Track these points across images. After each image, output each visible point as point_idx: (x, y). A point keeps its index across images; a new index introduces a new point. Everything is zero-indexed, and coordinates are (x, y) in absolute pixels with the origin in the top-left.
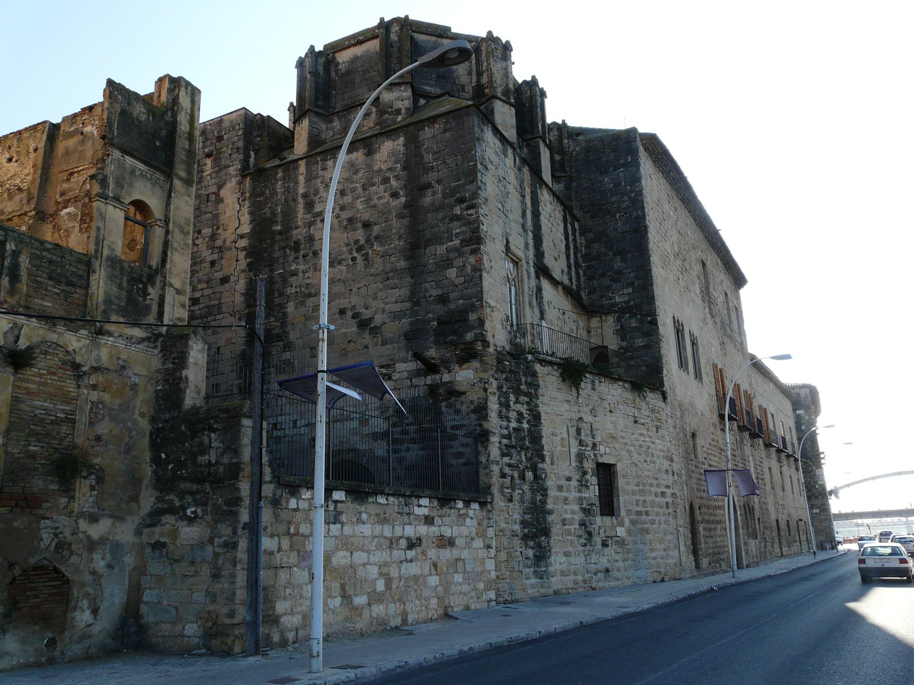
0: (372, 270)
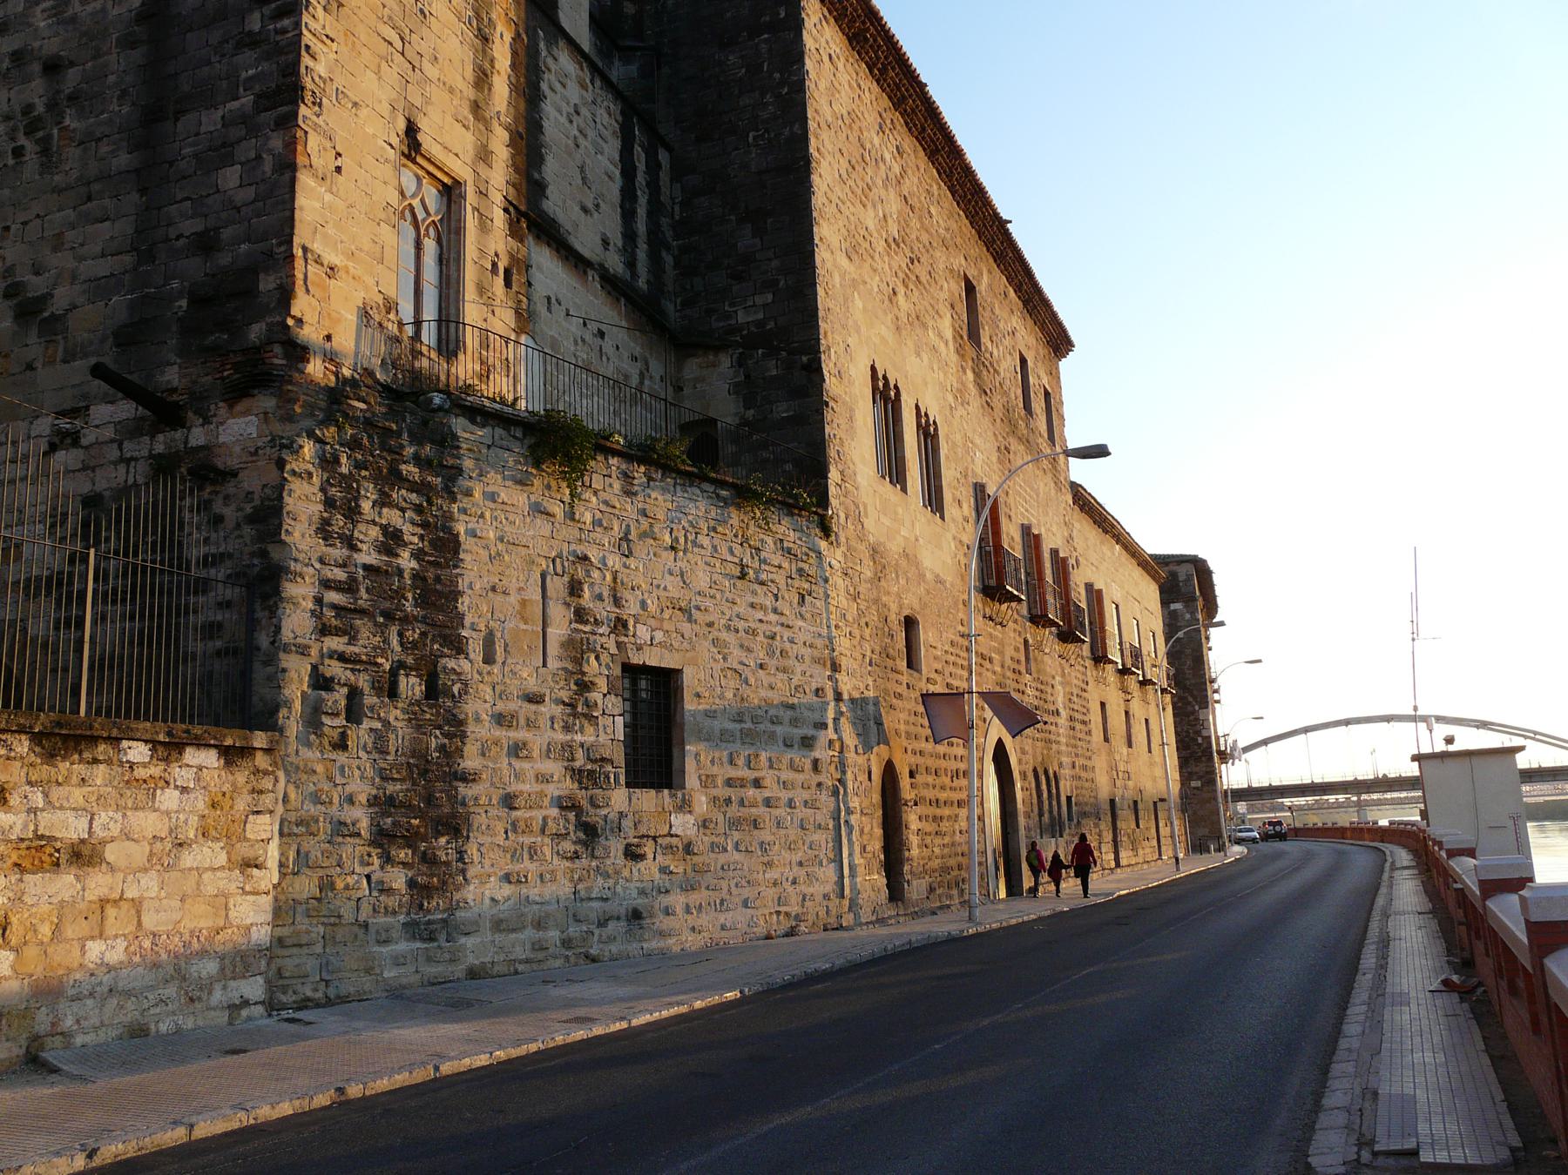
0: (56, 178)
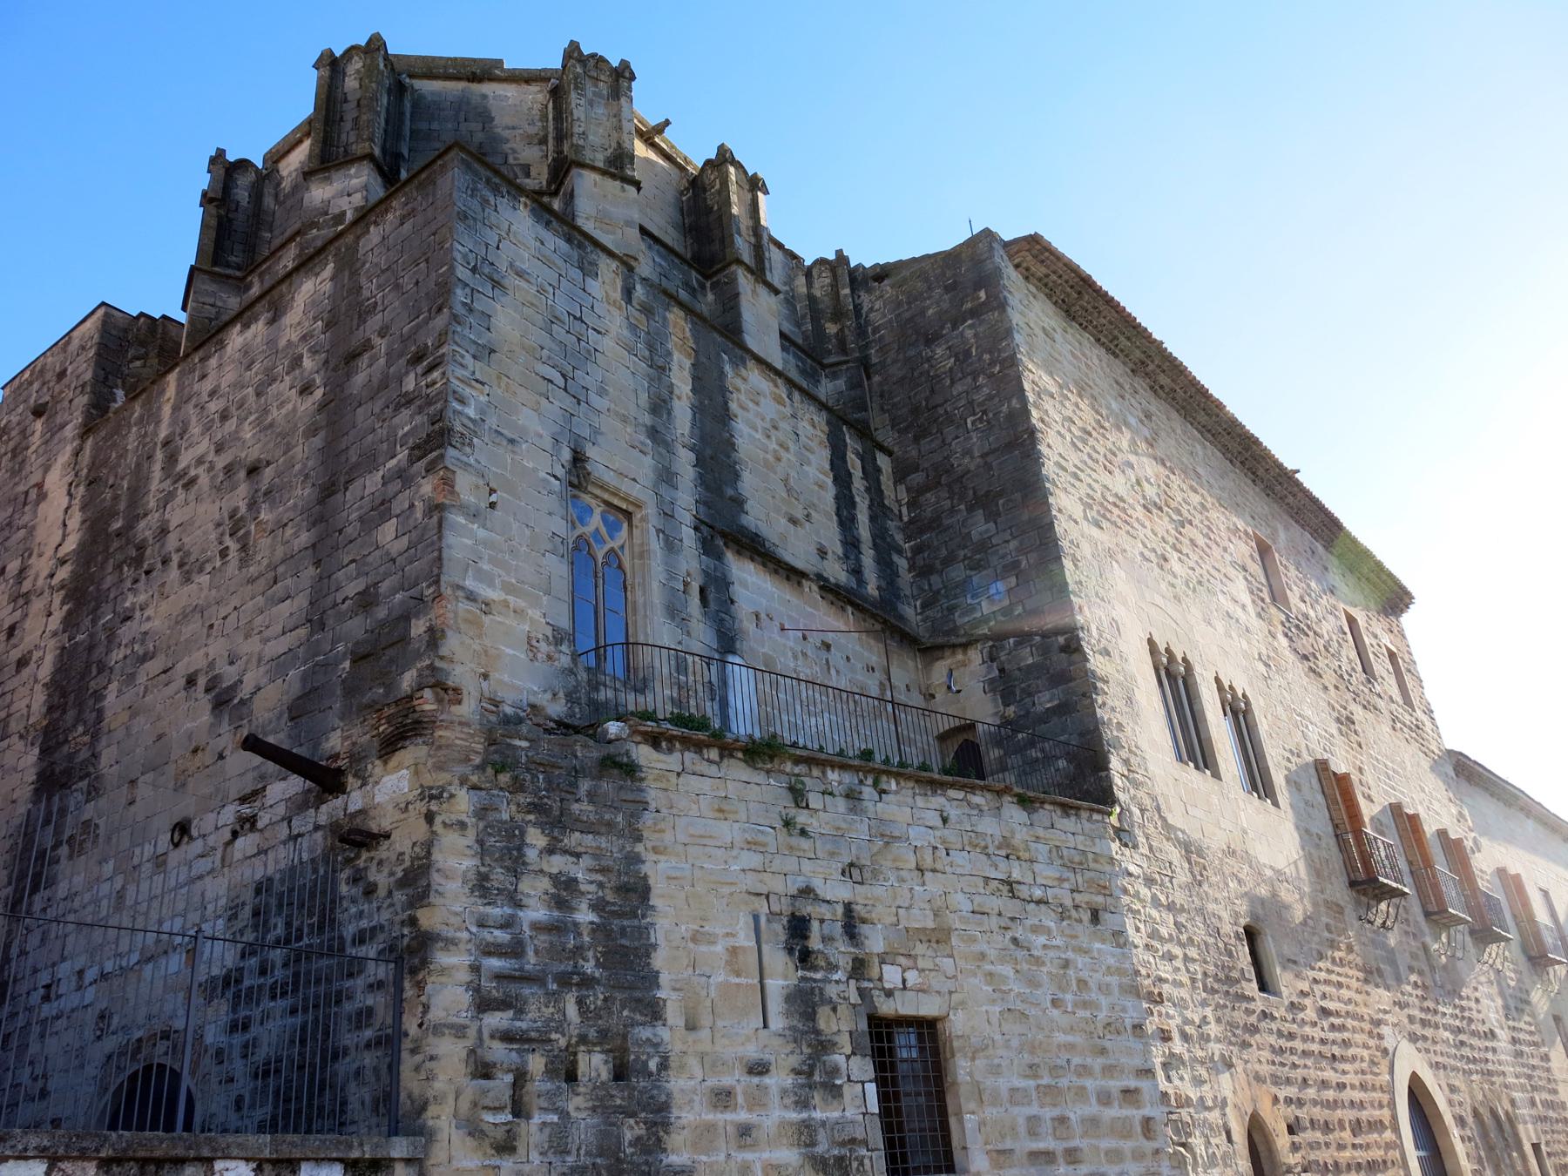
0: (251, 569)
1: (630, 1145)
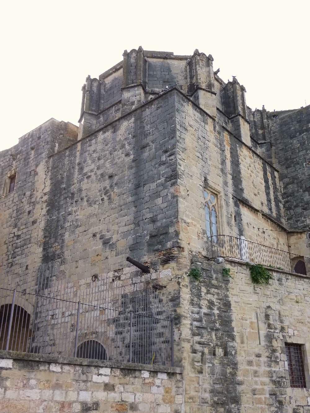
1: (229, 374)
